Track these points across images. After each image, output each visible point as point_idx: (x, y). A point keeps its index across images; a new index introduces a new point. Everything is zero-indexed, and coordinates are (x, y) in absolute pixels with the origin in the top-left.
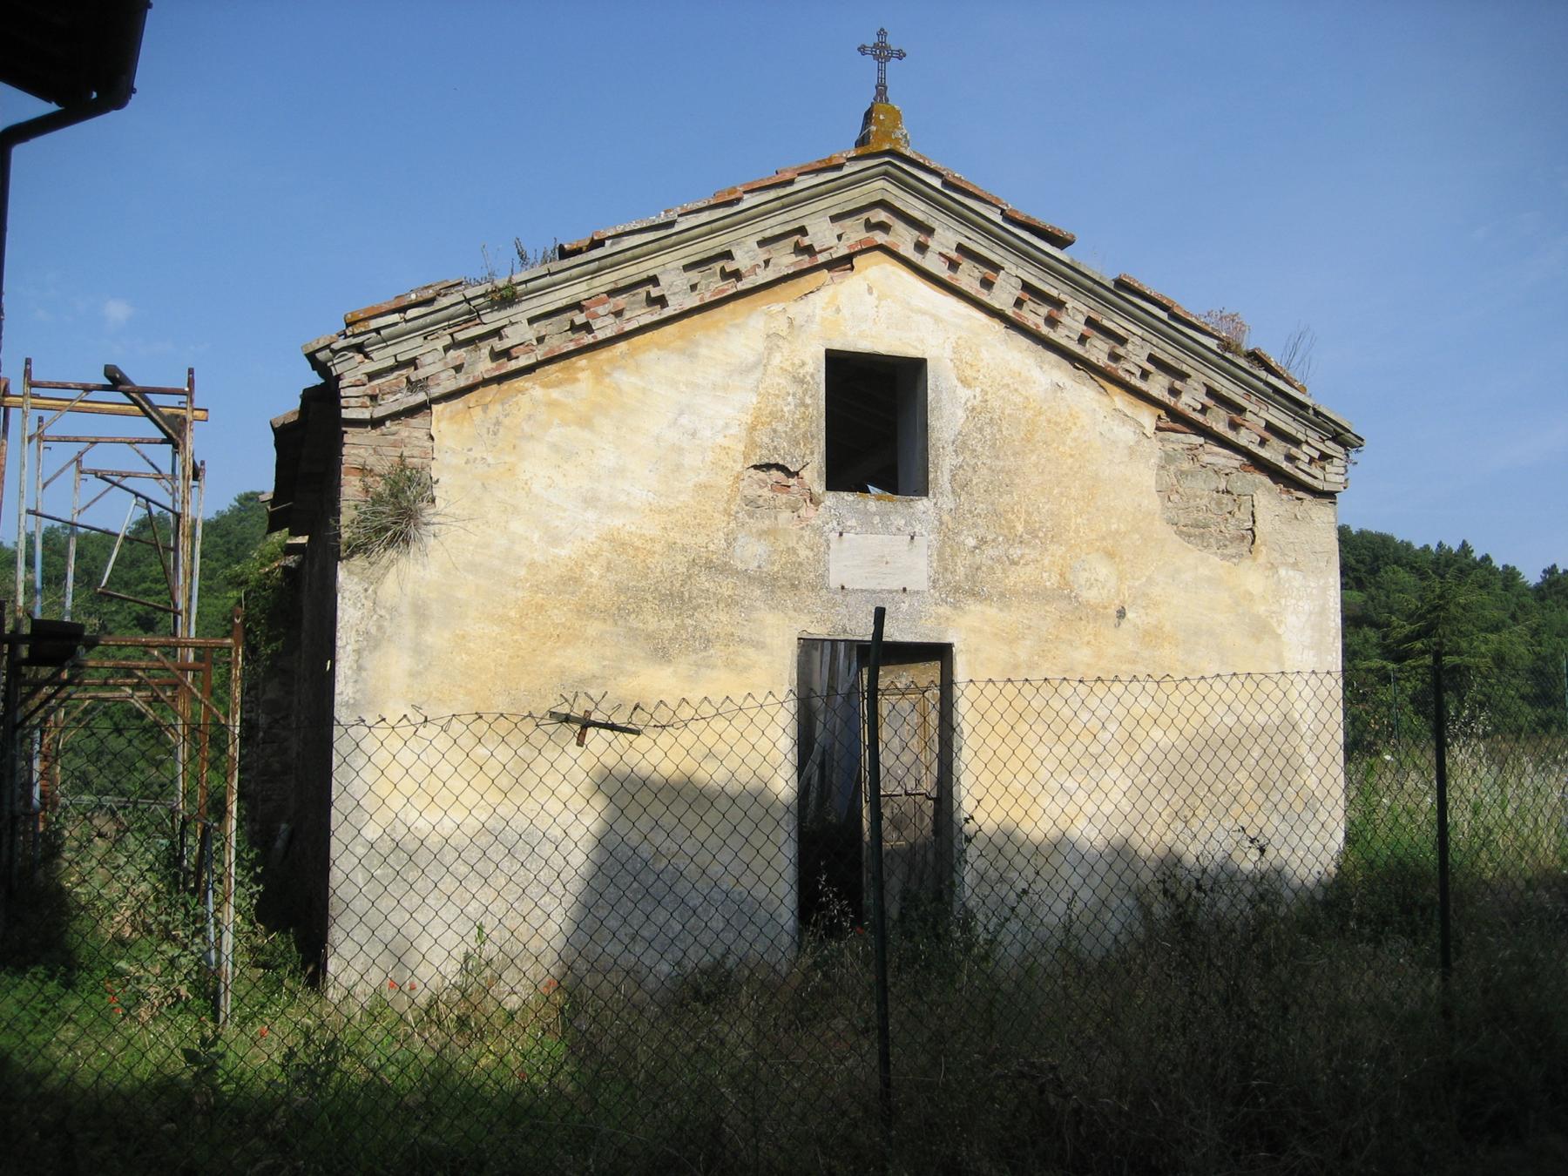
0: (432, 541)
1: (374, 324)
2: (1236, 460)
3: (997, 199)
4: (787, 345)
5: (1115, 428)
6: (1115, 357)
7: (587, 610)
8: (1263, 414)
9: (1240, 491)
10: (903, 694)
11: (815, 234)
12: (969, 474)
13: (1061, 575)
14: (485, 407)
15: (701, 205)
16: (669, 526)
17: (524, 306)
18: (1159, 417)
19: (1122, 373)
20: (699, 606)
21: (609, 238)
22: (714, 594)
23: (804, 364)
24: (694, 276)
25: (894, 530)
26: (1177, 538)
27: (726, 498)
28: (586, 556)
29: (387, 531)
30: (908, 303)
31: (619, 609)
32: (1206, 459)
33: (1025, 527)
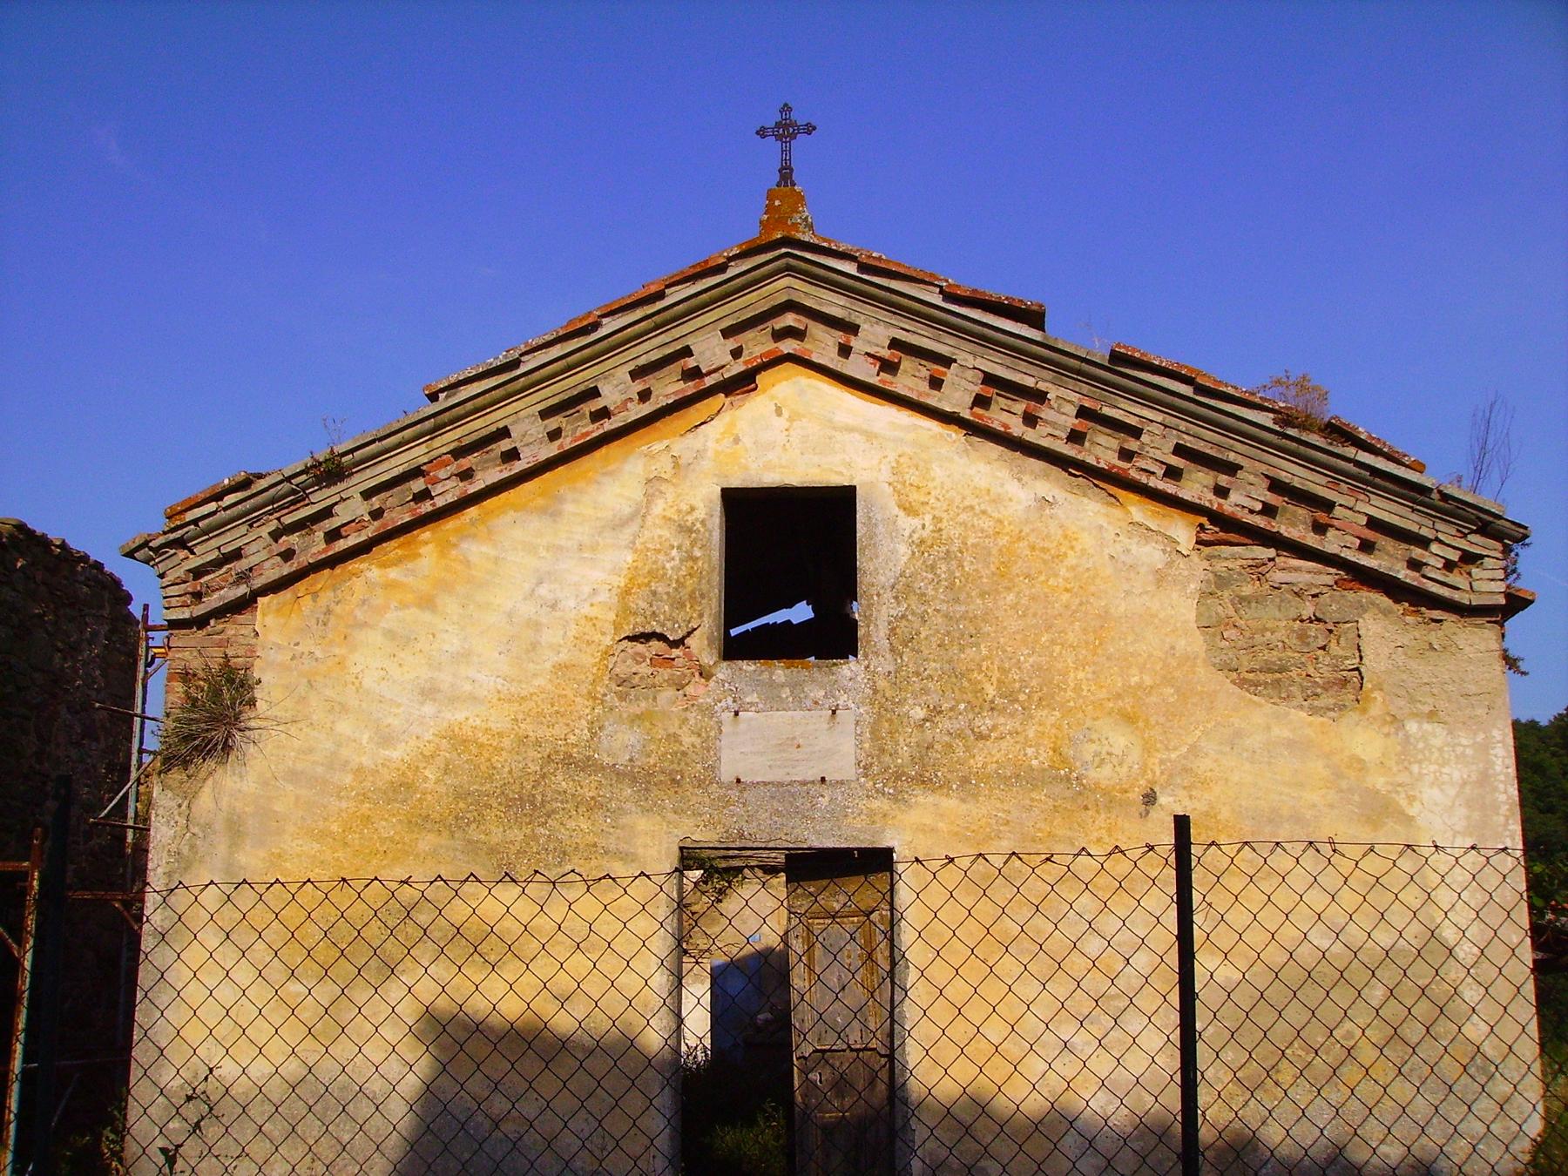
0: (252, 749)
1: (190, 516)
2: (1328, 575)
3: (931, 275)
4: (671, 489)
5: (1134, 548)
6: (1126, 455)
7: (421, 821)
8: (1360, 507)
9: (1336, 617)
10: (834, 917)
11: (702, 353)
12: (916, 625)
14: (315, 595)
15: (548, 338)
16: (520, 717)
17: (356, 479)
18: (1201, 526)
19: (1134, 474)
20: (554, 812)
21: (442, 390)
22: (573, 795)
23: (693, 509)
24: (554, 423)
25: (809, 703)
27: (591, 678)
28: (420, 757)
29: (195, 739)
30: (830, 421)
31: (457, 818)
32: (1278, 576)
33: (998, 688)
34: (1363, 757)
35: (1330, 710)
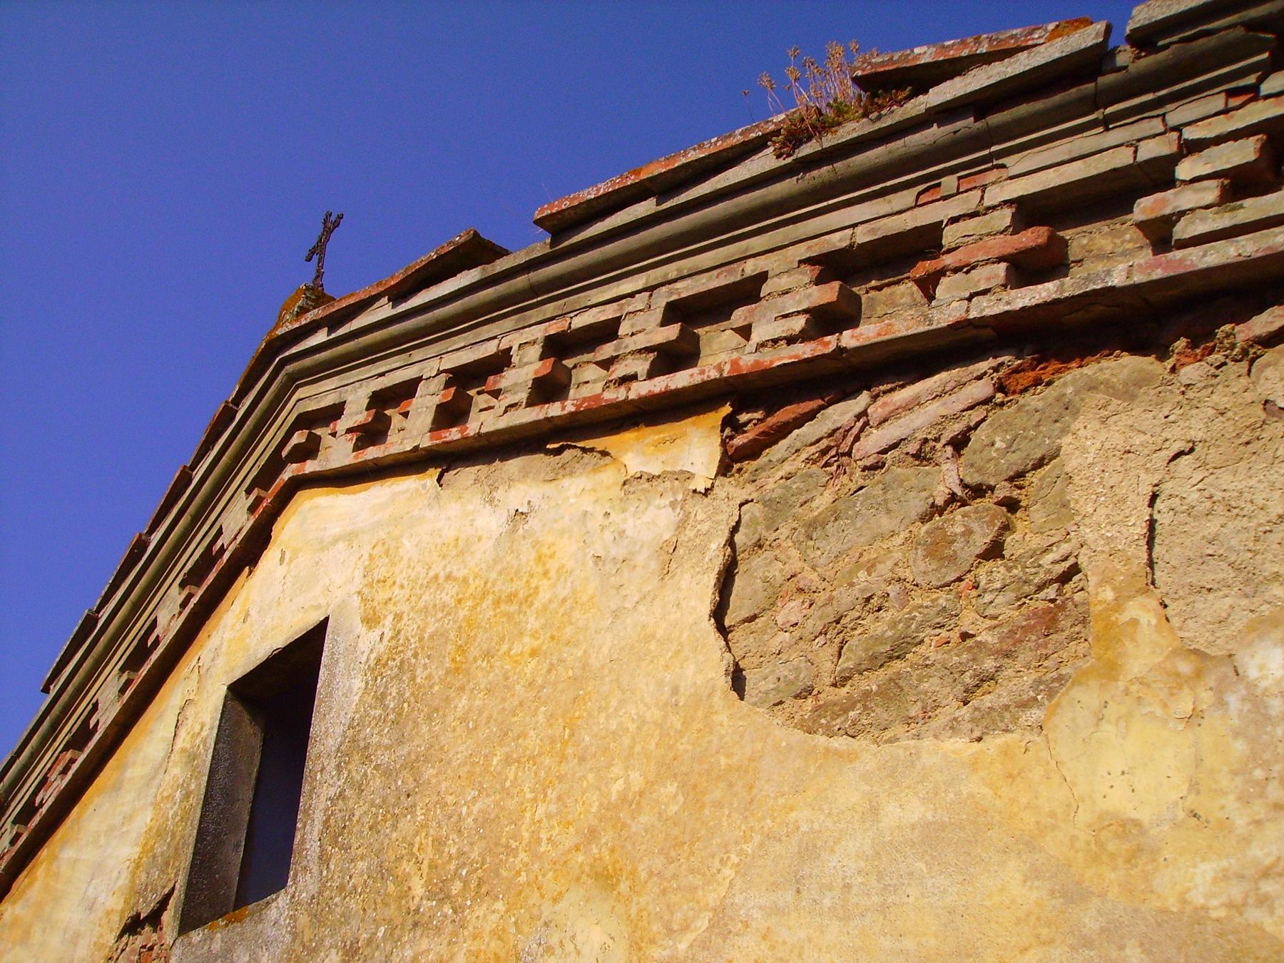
34: (1134, 815)
35: (1025, 705)
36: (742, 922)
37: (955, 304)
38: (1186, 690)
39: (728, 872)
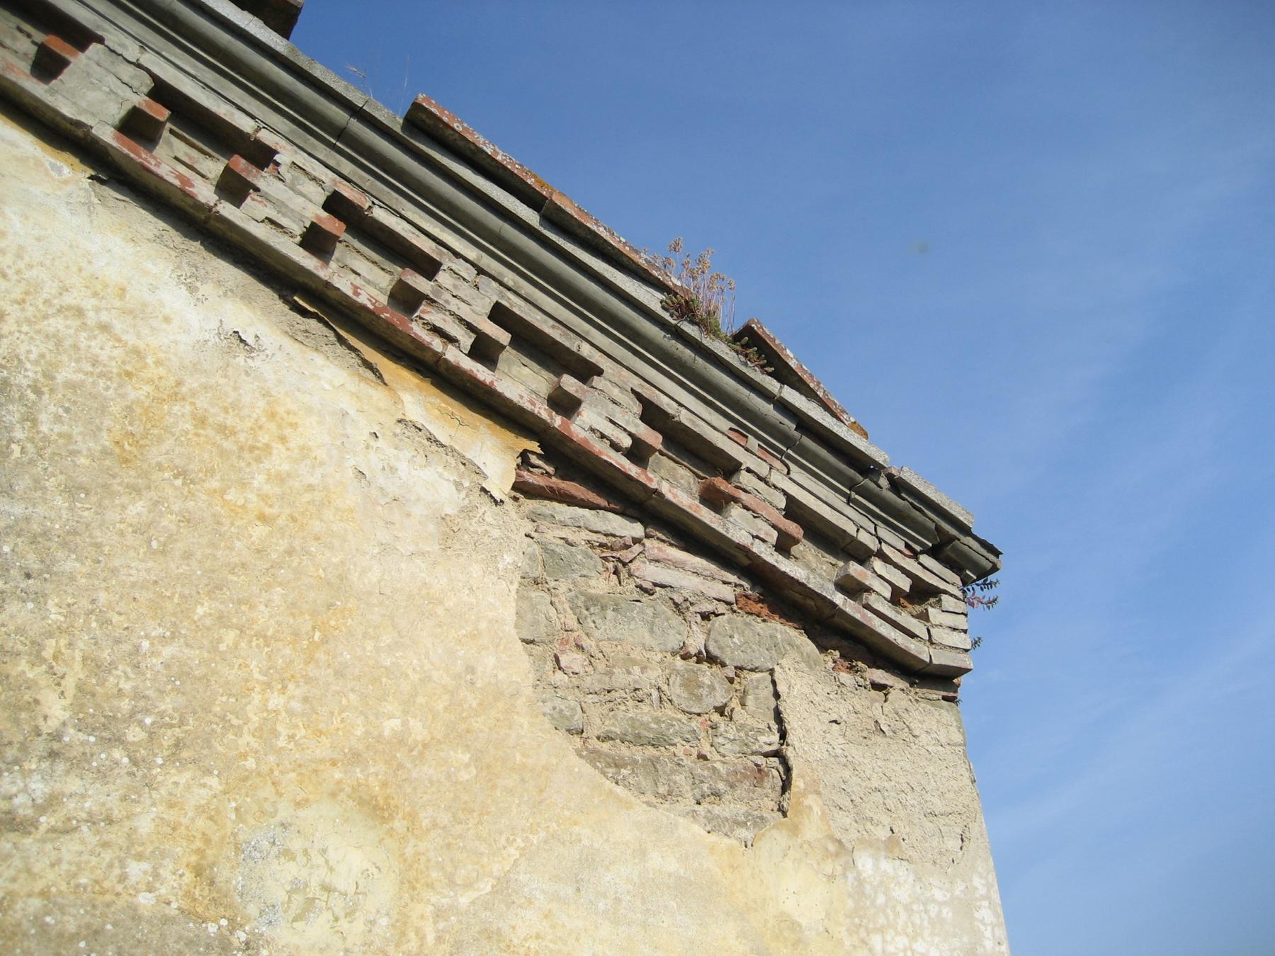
5: (403, 467)
9: (741, 659)
13: (198, 871)
26: (587, 769)
32: (650, 572)
33: (78, 707)
36: (525, 898)
37: (743, 531)
38: (830, 860)
39: (513, 852)
